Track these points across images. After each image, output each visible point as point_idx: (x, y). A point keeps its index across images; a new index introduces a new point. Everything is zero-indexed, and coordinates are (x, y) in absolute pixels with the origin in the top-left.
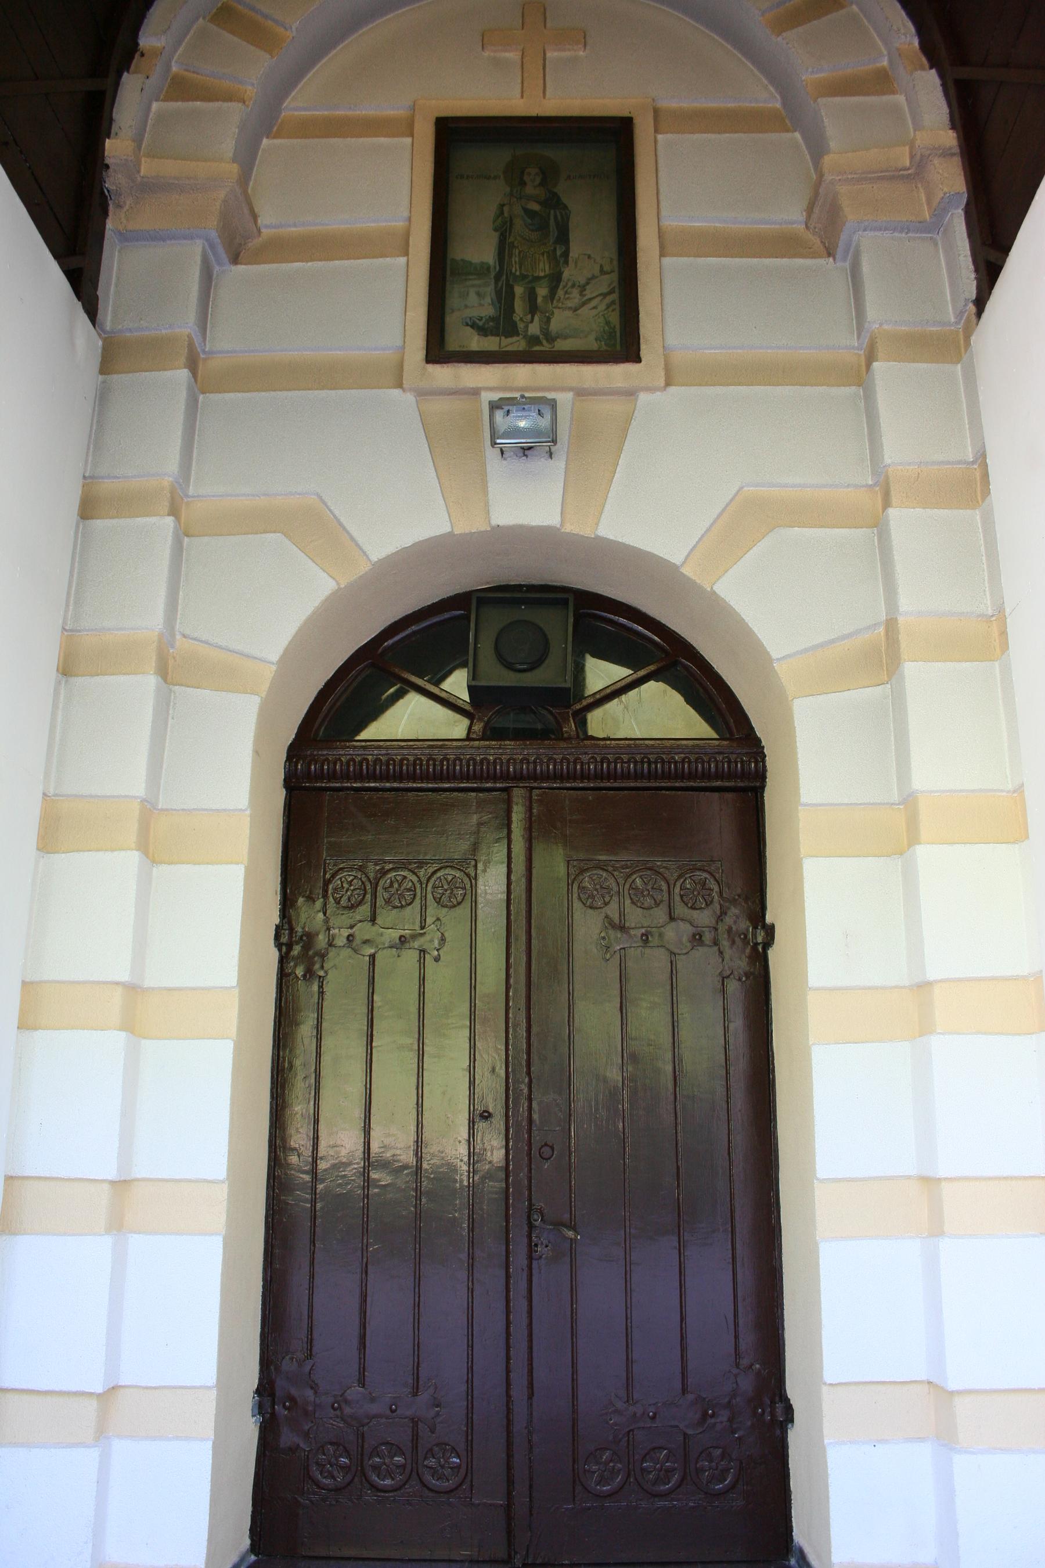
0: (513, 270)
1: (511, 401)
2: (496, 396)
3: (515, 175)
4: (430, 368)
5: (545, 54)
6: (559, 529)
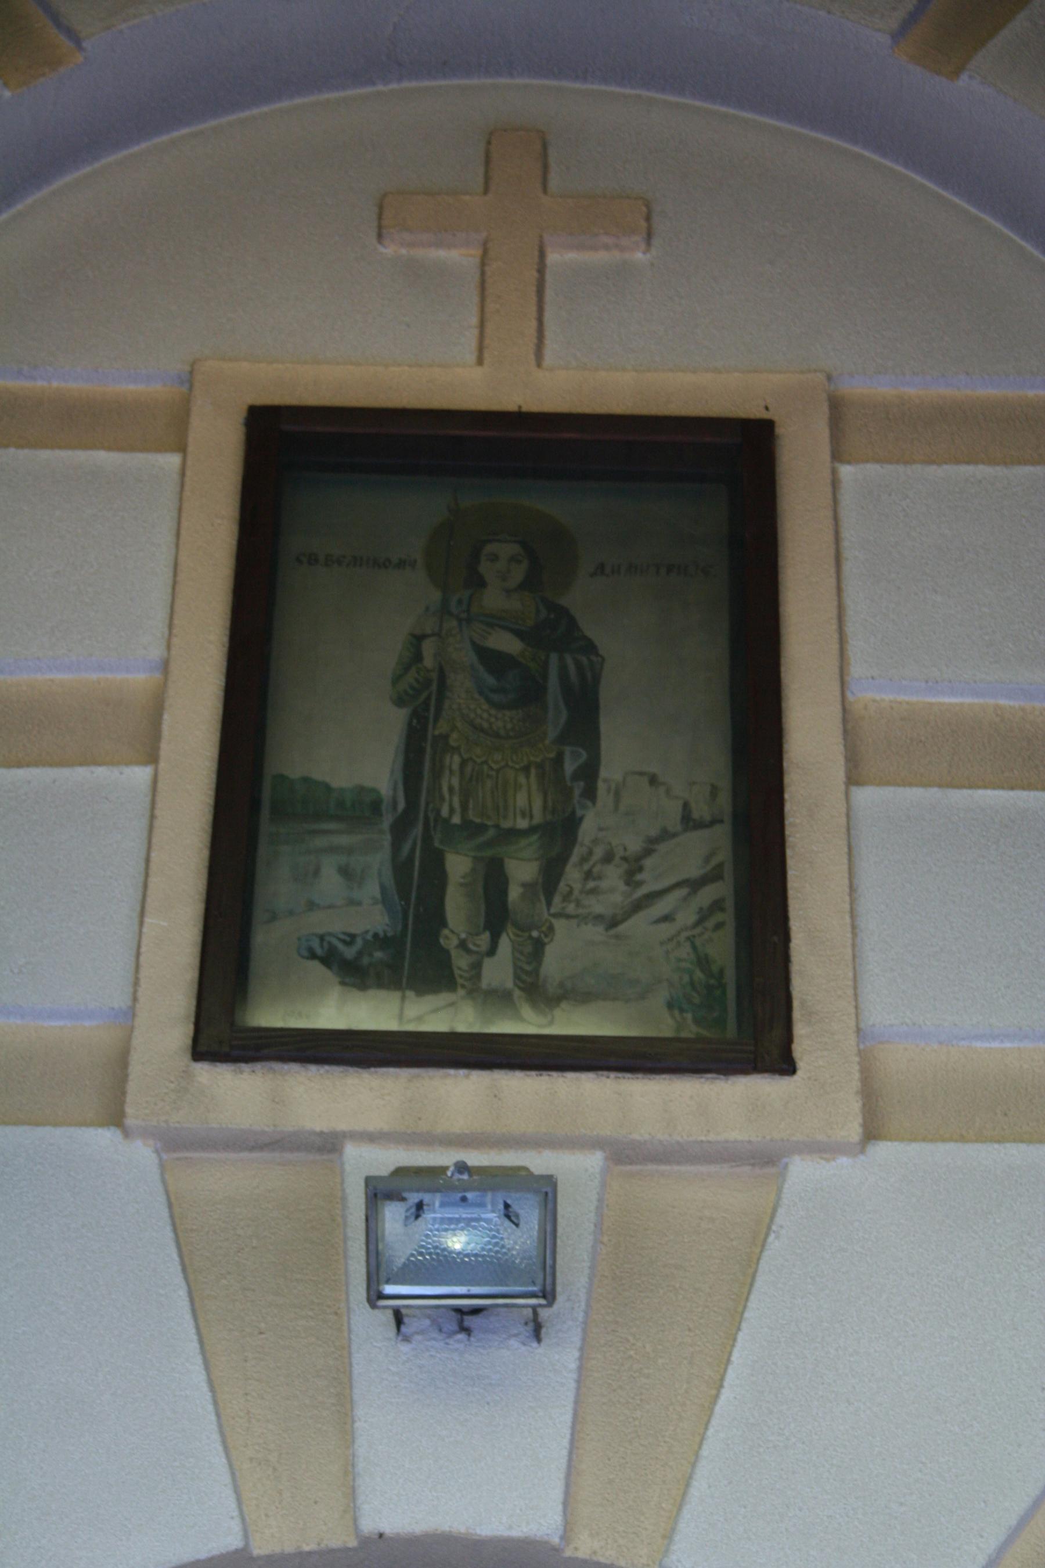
0: (445, 812)
1: (428, 1177)
2: (385, 1159)
3: (455, 563)
4: (205, 1073)
5: (542, 255)
6: (556, 1550)
